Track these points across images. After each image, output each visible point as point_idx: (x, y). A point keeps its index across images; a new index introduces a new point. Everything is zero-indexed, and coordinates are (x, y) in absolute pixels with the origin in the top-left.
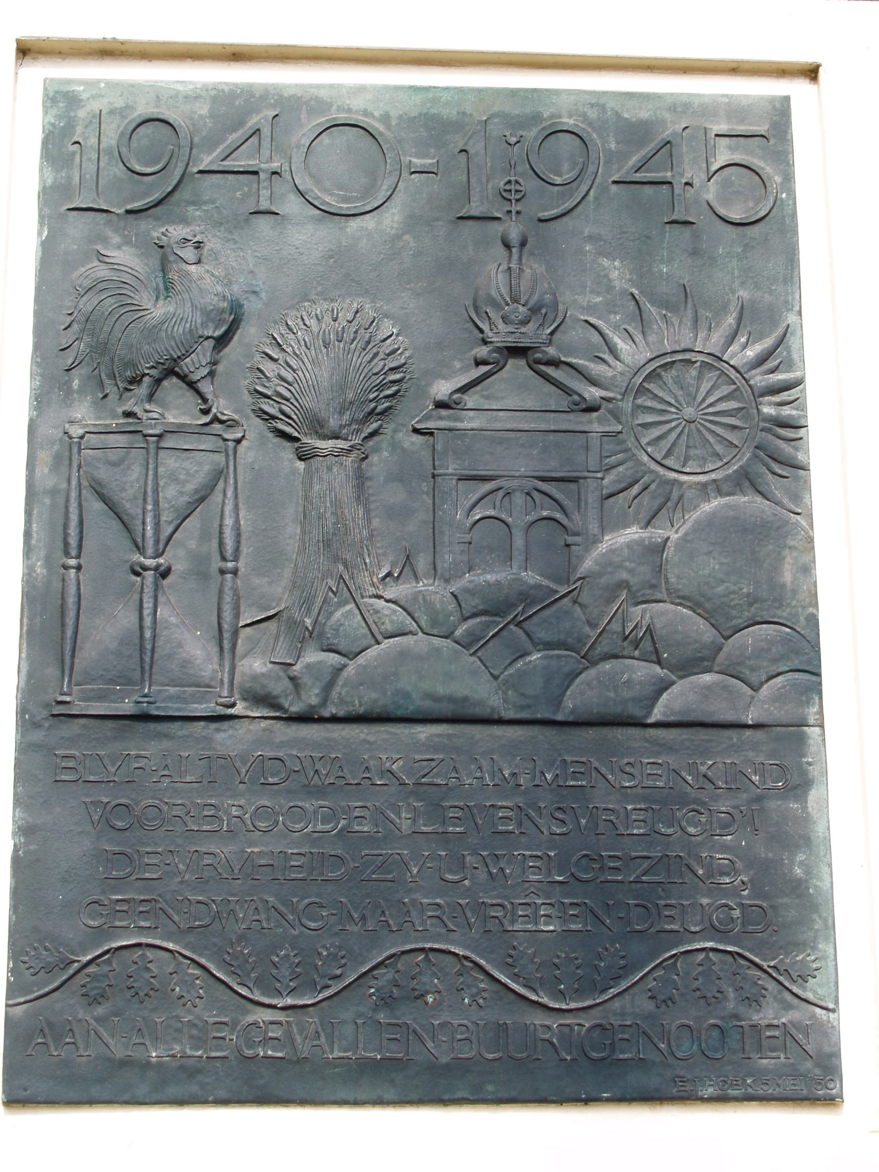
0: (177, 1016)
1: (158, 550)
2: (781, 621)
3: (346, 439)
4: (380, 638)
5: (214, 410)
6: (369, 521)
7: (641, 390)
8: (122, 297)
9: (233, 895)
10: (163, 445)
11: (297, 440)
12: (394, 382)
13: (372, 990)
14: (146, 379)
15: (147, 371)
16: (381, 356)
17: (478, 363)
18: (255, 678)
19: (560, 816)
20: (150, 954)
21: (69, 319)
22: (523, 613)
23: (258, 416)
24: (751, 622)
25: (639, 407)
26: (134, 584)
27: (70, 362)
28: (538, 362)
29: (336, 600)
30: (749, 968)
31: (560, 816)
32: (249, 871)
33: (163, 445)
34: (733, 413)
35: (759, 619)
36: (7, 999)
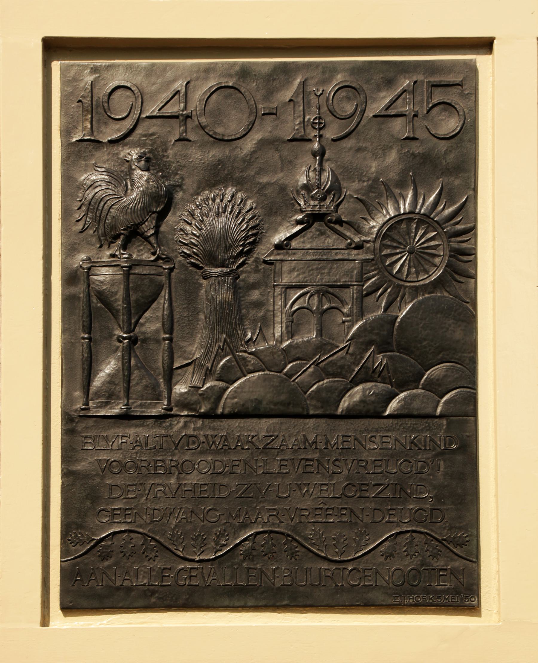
0: (145, 566)
1: (130, 329)
2: (456, 361)
3: (227, 267)
4: (246, 373)
5: (158, 253)
6: (240, 311)
7: (385, 236)
8: (107, 191)
9: (172, 505)
10: (133, 272)
11: (201, 268)
12: (252, 235)
13: (242, 552)
14: (122, 237)
15: (122, 232)
16: (246, 221)
17: (299, 222)
18: (182, 394)
20: (132, 535)
21: (80, 204)
22: (319, 358)
23: (181, 256)
24: (439, 361)
25: (384, 245)
26: (118, 347)
27: (81, 227)
28: (330, 221)
29: (223, 353)
30: (432, 540)
32: (180, 493)
33: (133, 272)
34: (434, 247)
35: (444, 360)
36: (61, 558)
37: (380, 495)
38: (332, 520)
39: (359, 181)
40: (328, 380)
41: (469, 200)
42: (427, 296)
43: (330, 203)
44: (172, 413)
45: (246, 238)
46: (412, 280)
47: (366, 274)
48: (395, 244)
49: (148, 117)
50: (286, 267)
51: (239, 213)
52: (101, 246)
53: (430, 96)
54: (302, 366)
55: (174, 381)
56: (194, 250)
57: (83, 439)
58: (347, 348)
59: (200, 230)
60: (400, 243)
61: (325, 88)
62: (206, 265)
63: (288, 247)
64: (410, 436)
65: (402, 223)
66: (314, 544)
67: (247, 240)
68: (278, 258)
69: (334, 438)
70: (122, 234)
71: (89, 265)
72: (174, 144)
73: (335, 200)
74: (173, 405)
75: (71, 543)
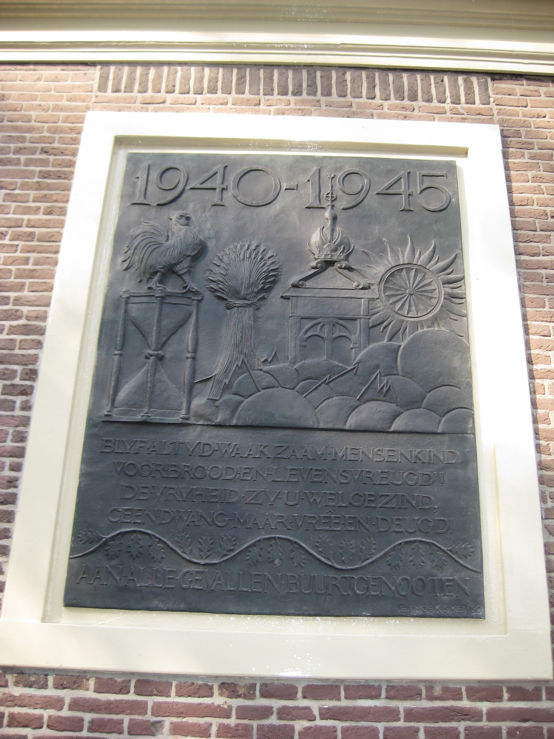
4: (260, 389)
11: (226, 300)
14: (159, 274)
19: (344, 474)
22: (330, 378)
25: (387, 288)
31: (344, 474)
36: (70, 555)
37: (277, 384)
38: (339, 529)
39: (365, 239)
40: (338, 397)
41: (457, 257)
42: (425, 329)
43: (340, 253)
44: (189, 422)
45: (267, 277)
46: (412, 316)
47: (372, 309)
48: (397, 288)
49: (191, 189)
50: (301, 302)
51: (262, 259)
52: (141, 281)
53: (422, 182)
54: (312, 384)
55: (194, 393)
56: (220, 286)
57: (104, 442)
58: (355, 369)
59: (227, 270)
60: (401, 287)
61: (336, 174)
62: (231, 298)
63: (303, 287)
64: (415, 451)
65: (402, 271)
66: (320, 552)
67: (267, 279)
68: (294, 294)
69: (341, 450)
70: (159, 271)
71: (128, 295)
72: (210, 208)
73: (345, 251)
74: (191, 415)
75: (81, 541)
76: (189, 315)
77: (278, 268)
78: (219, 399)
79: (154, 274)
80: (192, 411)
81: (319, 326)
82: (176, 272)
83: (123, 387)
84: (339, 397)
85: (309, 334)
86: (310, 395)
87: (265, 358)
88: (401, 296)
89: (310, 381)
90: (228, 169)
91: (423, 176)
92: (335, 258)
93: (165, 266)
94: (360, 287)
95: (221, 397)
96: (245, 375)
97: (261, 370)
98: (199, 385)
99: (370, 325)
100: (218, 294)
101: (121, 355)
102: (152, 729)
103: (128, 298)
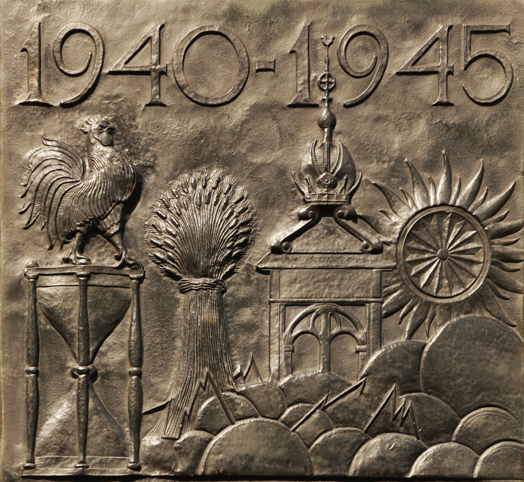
4: (233, 419)
11: (179, 278)
14: (78, 235)
22: (326, 400)
25: (409, 248)
40: (338, 429)
42: (462, 316)
44: (140, 473)
45: (235, 237)
50: (285, 277)
51: (226, 204)
52: (51, 248)
53: (469, 47)
55: (143, 429)
60: (429, 246)
61: (336, 36)
62: (185, 274)
63: (288, 251)
67: (236, 241)
68: (276, 264)
72: (144, 110)
73: (348, 186)
74: (141, 462)
76: (127, 304)
77: (251, 220)
78: (179, 437)
79: (71, 235)
80: (141, 457)
81: (314, 314)
82: (103, 233)
83: (43, 423)
84: (340, 429)
85: (296, 332)
86: (301, 426)
87: (238, 370)
88: (428, 263)
89: (300, 405)
90: (167, 28)
91: (473, 32)
92: (333, 200)
93: (86, 222)
94: (370, 249)
95: (180, 434)
96: (211, 399)
97: (233, 391)
98: (150, 417)
99: (384, 312)
100: (167, 268)
101: (37, 373)
102: (382, 385)
103: (36, 278)
